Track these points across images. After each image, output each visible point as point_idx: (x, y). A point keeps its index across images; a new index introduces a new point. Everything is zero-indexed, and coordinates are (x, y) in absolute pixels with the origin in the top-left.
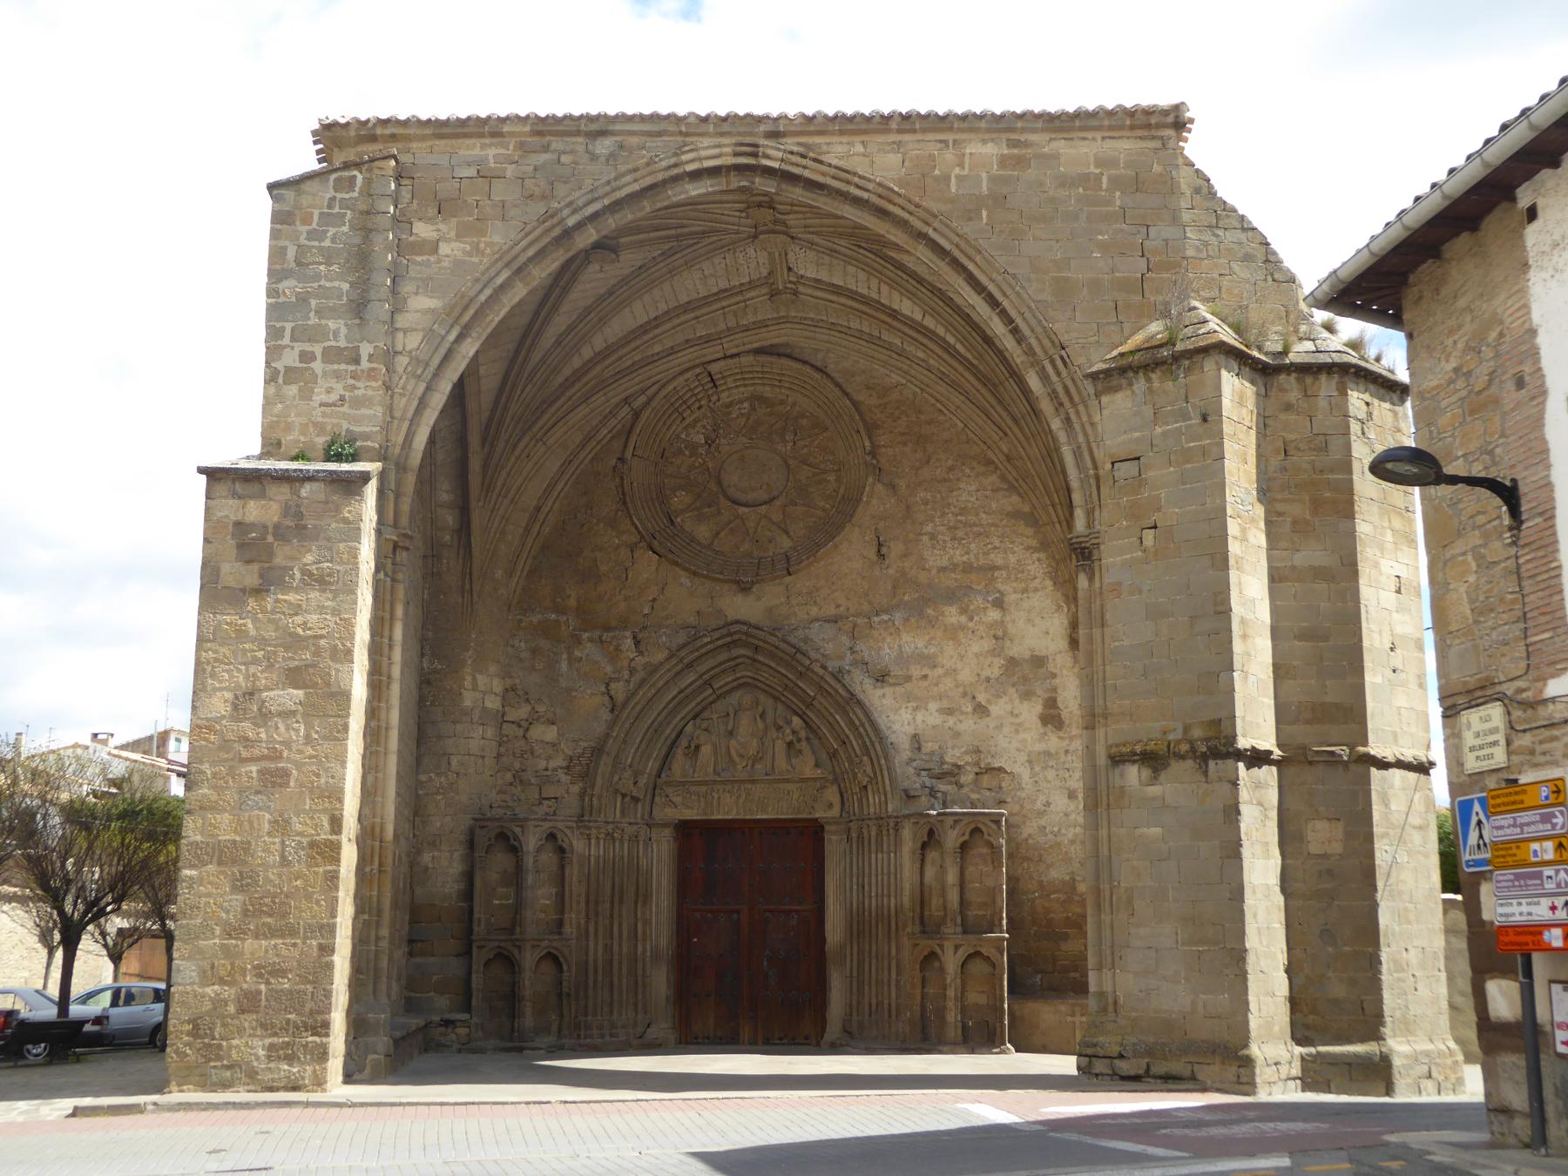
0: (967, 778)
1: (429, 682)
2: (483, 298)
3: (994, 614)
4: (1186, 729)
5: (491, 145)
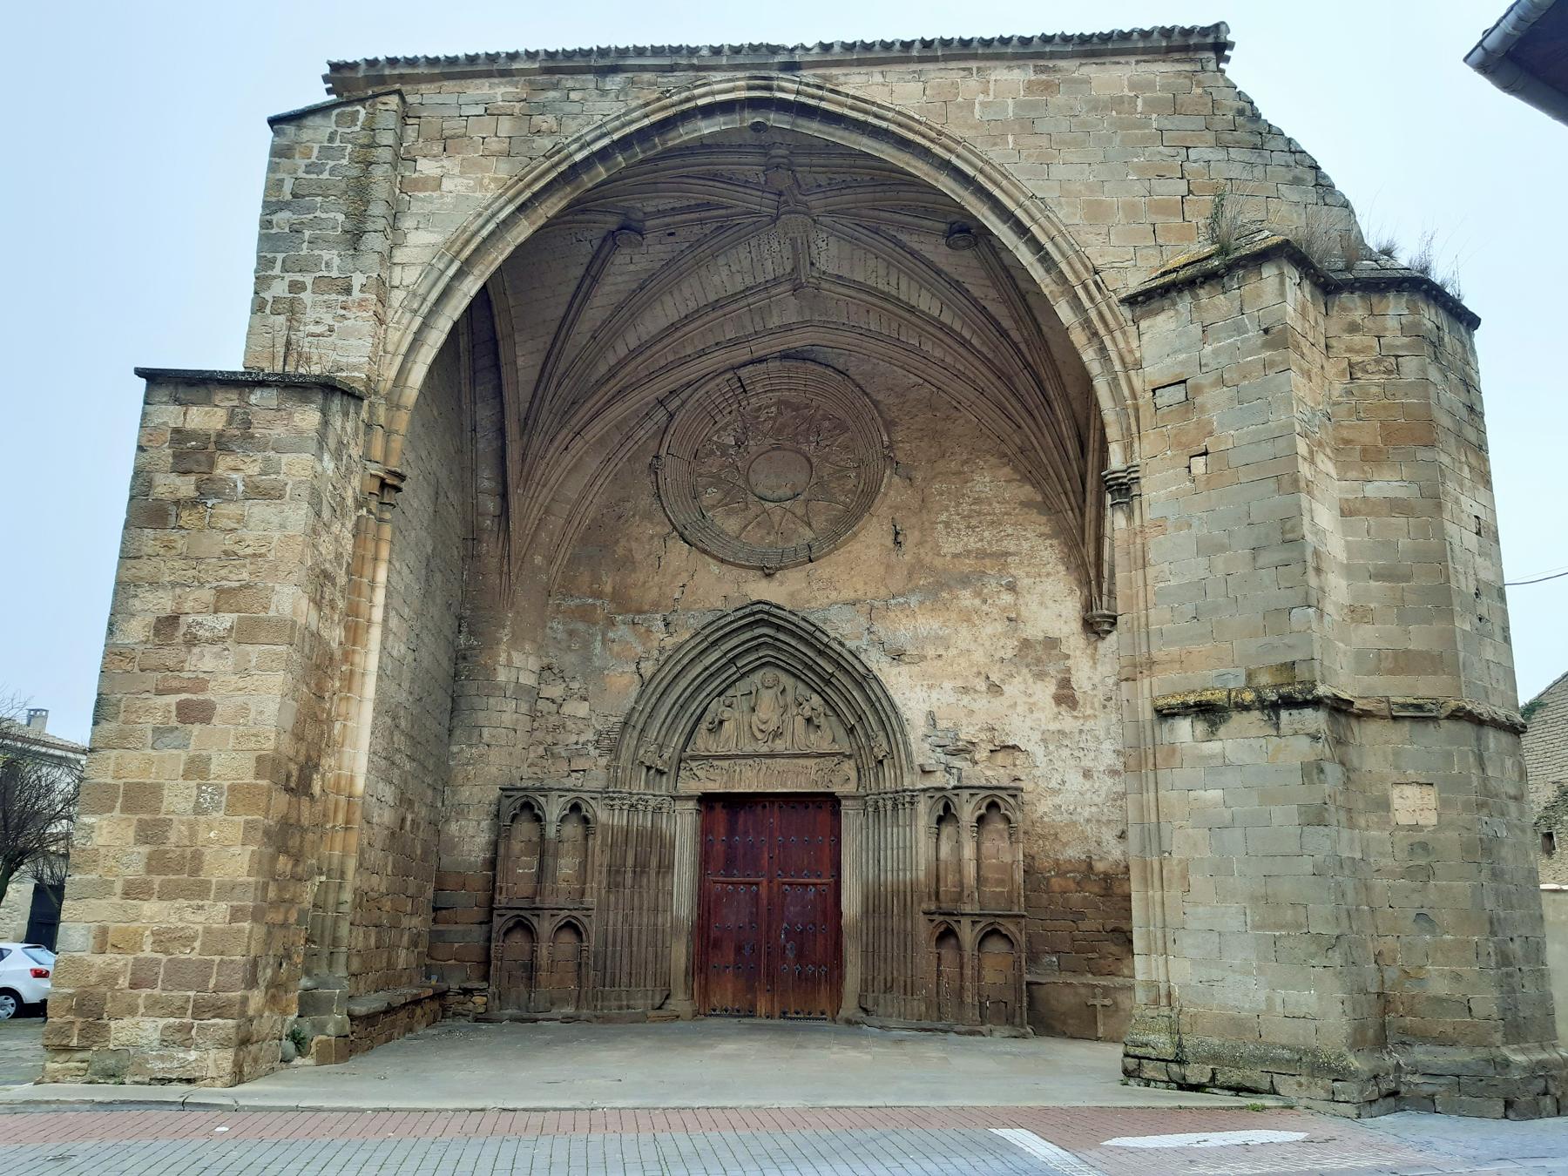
0: (981, 754)
1: (465, 658)
2: (485, 233)
3: (1007, 598)
4: (1250, 676)
5: (498, 85)
